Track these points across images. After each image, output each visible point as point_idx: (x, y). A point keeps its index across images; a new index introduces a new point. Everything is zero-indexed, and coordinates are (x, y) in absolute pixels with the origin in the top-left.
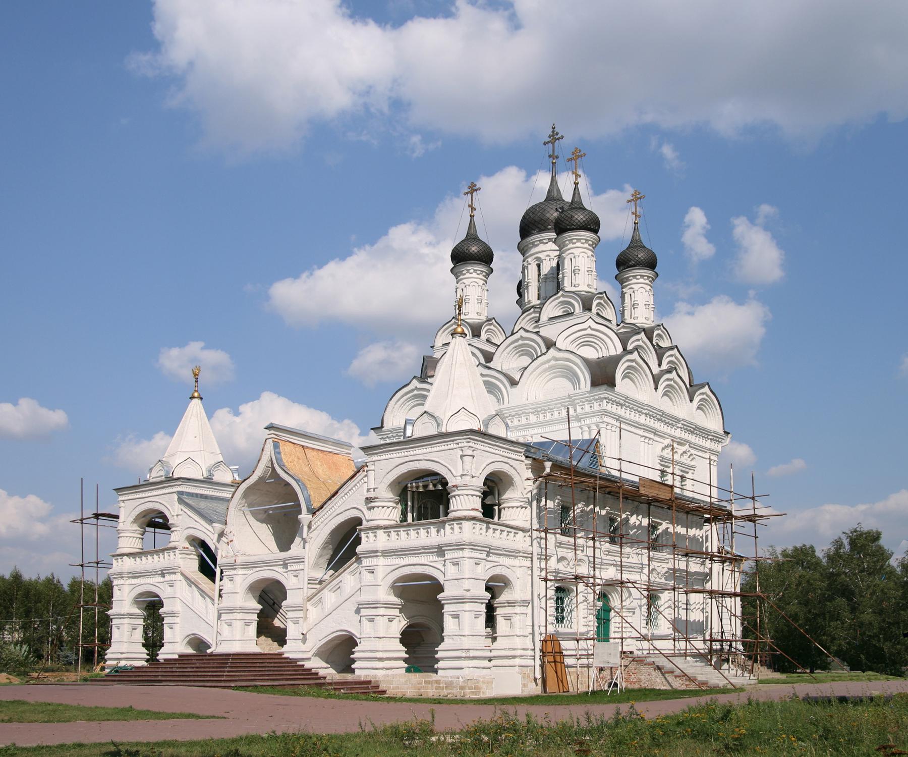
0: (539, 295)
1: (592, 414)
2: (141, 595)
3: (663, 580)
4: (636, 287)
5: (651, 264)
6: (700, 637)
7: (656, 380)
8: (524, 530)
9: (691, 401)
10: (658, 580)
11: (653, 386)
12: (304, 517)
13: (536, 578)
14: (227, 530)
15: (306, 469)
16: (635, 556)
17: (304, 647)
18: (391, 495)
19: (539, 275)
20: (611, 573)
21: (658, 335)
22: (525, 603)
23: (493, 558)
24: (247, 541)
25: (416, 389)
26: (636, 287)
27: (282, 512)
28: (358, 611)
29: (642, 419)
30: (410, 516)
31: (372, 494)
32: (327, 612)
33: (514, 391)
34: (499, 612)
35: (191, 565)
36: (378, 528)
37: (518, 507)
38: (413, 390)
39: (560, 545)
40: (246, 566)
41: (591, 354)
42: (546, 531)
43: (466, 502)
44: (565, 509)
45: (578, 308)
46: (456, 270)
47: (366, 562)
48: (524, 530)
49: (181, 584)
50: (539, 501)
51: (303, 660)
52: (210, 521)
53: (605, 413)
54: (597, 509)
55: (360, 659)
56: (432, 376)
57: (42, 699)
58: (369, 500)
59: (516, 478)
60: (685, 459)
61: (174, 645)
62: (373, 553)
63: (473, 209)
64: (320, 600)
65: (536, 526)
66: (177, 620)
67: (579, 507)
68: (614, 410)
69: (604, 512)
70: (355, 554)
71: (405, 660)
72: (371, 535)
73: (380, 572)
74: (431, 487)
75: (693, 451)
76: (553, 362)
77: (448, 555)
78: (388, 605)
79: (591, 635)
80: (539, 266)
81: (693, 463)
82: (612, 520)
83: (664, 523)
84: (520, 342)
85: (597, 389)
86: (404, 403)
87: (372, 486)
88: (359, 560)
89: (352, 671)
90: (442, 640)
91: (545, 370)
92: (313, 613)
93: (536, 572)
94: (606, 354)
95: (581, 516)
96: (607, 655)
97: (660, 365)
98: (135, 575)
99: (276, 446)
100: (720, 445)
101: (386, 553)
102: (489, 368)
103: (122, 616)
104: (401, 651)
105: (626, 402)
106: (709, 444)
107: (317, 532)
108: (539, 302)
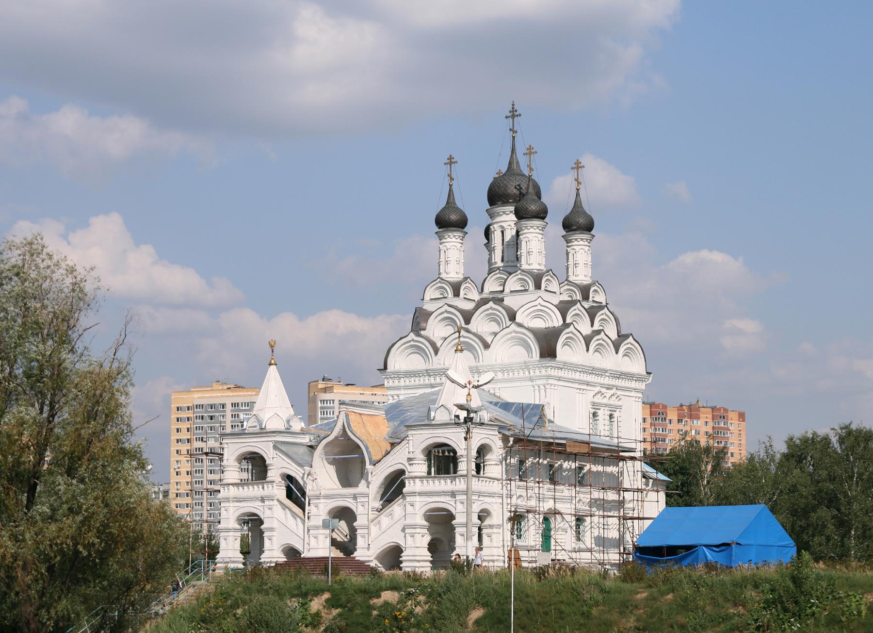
0: (503, 257)
1: (541, 378)
3: (587, 508)
5: (588, 227)
6: (617, 551)
7: (588, 340)
8: (498, 480)
9: (617, 353)
10: (583, 507)
11: (585, 348)
12: (368, 466)
13: (505, 510)
14: (313, 471)
15: (363, 431)
16: (565, 491)
17: (368, 553)
18: (422, 457)
19: (503, 240)
20: (548, 505)
21: (595, 291)
22: (498, 526)
23: (481, 498)
24: (322, 479)
25: (413, 340)
27: (349, 460)
28: (403, 530)
29: (577, 376)
30: (433, 469)
31: (411, 456)
32: (383, 530)
33: (486, 353)
34: (484, 531)
35: (282, 493)
36: (416, 477)
37: (494, 468)
38: (410, 341)
39: (519, 487)
40: (327, 497)
42: (510, 480)
44: (522, 462)
45: (531, 286)
47: (408, 499)
48: (498, 480)
49: (277, 508)
50: (506, 460)
51: (369, 561)
52: (301, 465)
53: (549, 377)
54: (541, 461)
55: (406, 561)
56: (425, 329)
58: (409, 459)
59: (493, 447)
60: (613, 401)
61: (272, 554)
62: (413, 494)
63: (452, 179)
64: (379, 523)
65: (504, 477)
66: (275, 533)
67: (529, 462)
68: (556, 374)
69: (545, 462)
70: (402, 493)
71: (431, 562)
72: (412, 481)
73: (418, 506)
74: (447, 454)
75: (619, 393)
76: (513, 334)
77: (458, 497)
78: (422, 527)
79: (537, 547)
80: (503, 232)
81: (620, 403)
82: (551, 466)
83: (588, 465)
84: (490, 311)
85: (543, 359)
86: (403, 351)
87: (411, 450)
88: (404, 497)
89: (401, 569)
91: (508, 340)
92: (374, 530)
93: (505, 506)
94: (551, 325)
95: (531, 467)
96: (544, 560)
97: (592, 326)
98: (239, 500)
99: (347, 416)
100: (644, 384)
101: (421, 494)
102: (468, 331)
103: (228, 530)
104: (428, 556)
105: (566, 366)
106: (633, 384)
107: (377, 475)
108: (502, 265)
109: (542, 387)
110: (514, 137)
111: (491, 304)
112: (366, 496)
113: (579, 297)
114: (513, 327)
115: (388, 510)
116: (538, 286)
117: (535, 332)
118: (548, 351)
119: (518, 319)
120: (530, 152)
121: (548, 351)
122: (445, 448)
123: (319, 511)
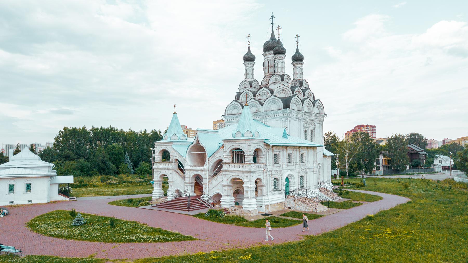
2: (162, 175)
4: (297, 67)
9: (314, 106)
26: (297, 67)
35: (176, 167)
41: (283, 95)
43: (249, 159)
97: (304, 96)
107: (210, 164)
111: (264, 88)
113: (298, 84)
114: (273, 97)
115: (215, 178)
116: (282, 80)
117: (282, 99)
118: (287, 105)
119: (275, 93)
120: (279, 28)
121: (287, 105)
123: (189, 176)
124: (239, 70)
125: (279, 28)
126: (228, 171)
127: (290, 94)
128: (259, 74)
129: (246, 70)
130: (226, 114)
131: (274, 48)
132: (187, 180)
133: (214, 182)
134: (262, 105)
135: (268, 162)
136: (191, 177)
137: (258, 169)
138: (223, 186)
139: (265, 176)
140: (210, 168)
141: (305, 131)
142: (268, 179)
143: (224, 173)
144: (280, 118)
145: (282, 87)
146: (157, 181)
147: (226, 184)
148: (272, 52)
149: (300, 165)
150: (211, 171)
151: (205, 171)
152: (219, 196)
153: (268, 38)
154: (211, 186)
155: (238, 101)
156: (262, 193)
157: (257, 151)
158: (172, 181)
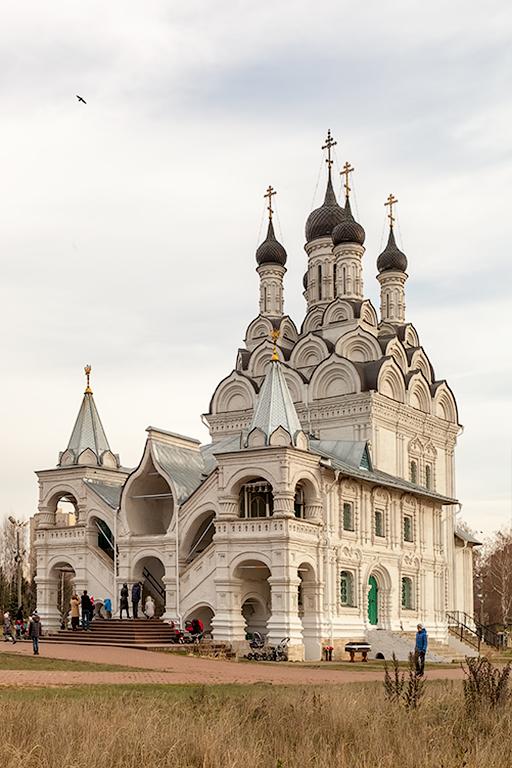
9: (433, 396)
41: (359, 358)
46: (260, 270)
57: (55, 673)
63: (271, 212)
90: (270, 613)
102: (288, 367)
107: (180, 526)
109: (362, 426)
110: (330, 168)
112: (169, 547)
116: (357, 315)
119: (338, 351)
120: (347, 169)
122: (259, 483)
124: (241, 292)
125: (347, 169)
126: (230, 542)
127: (377, 355)
128: (296, 307)
129: (264, 289)
130: (214, 411)
131: (334, 226)
132: (125, 574)
133: (194, 575)
134: (306, 382)
135: (328, 523)
136: (133, 565)
137: (306, 536)
138: (218, 583)
139: (321, 558)
140: (183, 536)
141: (413, 464)
142: (329, 571)
143: (219, 548)
144: (352, 417)
145: (356, 333)
146: (46, 582)
147: (225, 578)
148: (329, 240)
149: (402, 546)
150: (184, 547)
151: (169, 547)
152: (207, 612)
153: (319, 202)
154: (186, 588)
155: (244, 372)
156: (313, 606)
157: (303, 486)
158: (83, 578)
